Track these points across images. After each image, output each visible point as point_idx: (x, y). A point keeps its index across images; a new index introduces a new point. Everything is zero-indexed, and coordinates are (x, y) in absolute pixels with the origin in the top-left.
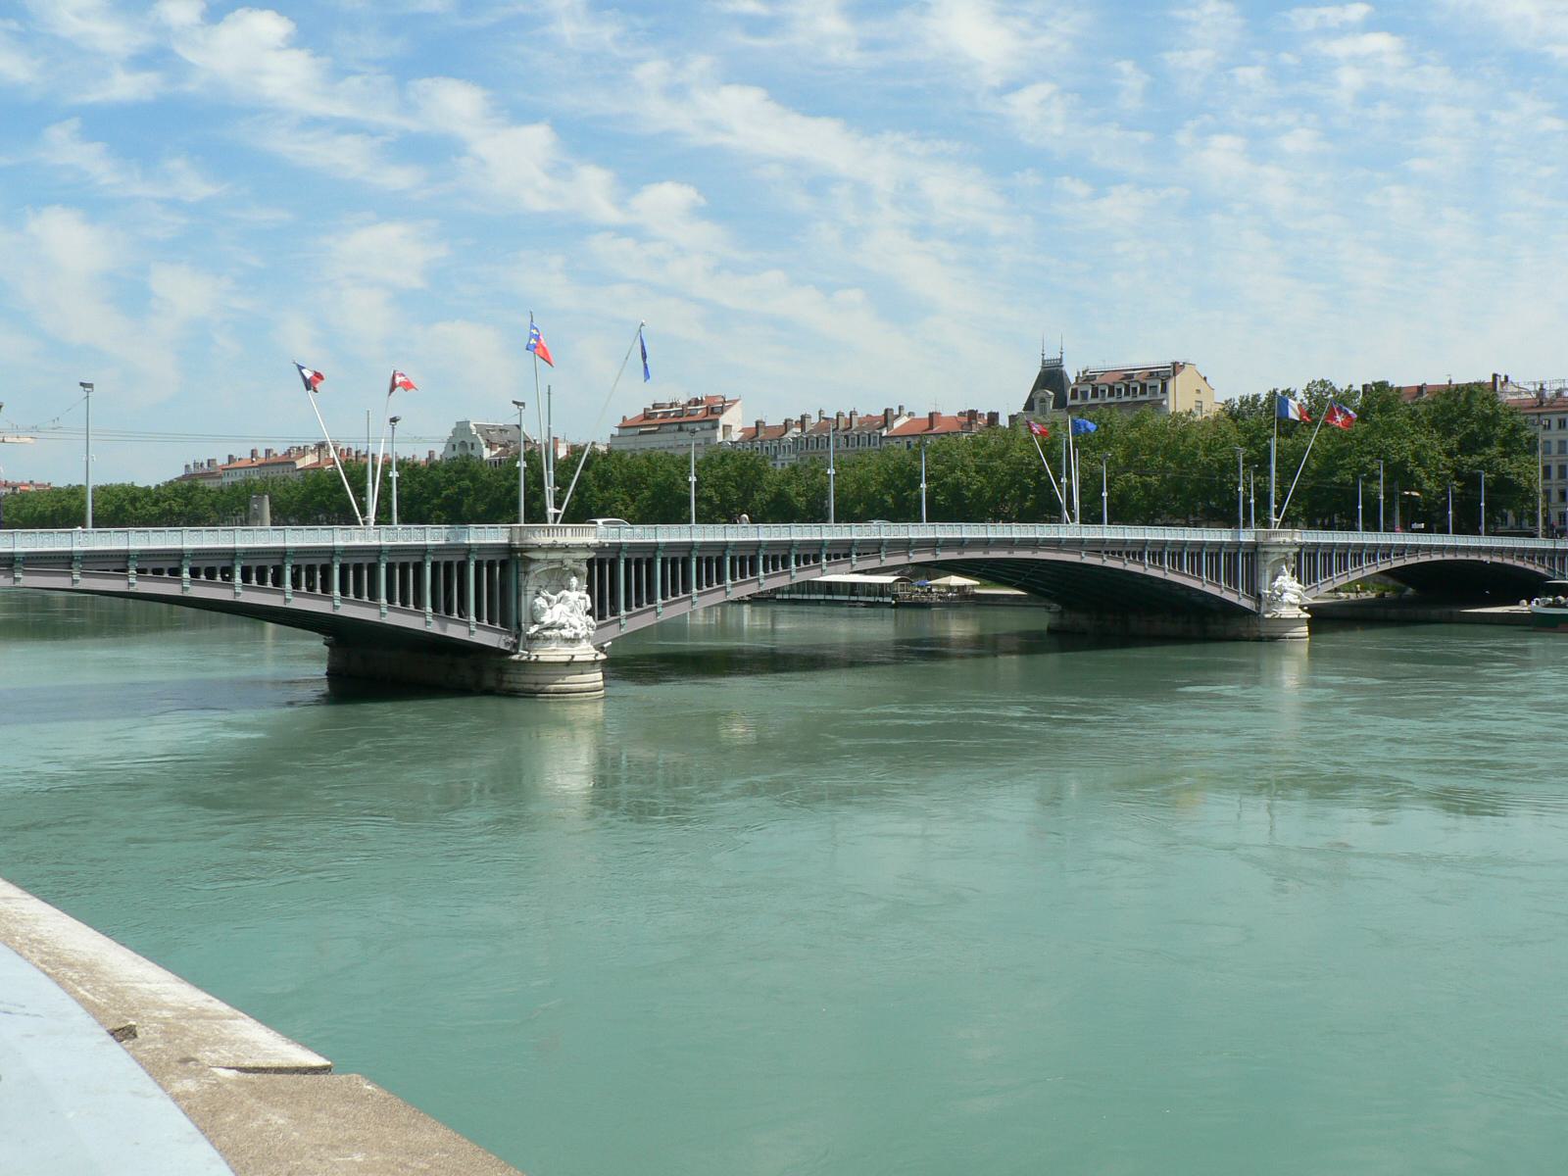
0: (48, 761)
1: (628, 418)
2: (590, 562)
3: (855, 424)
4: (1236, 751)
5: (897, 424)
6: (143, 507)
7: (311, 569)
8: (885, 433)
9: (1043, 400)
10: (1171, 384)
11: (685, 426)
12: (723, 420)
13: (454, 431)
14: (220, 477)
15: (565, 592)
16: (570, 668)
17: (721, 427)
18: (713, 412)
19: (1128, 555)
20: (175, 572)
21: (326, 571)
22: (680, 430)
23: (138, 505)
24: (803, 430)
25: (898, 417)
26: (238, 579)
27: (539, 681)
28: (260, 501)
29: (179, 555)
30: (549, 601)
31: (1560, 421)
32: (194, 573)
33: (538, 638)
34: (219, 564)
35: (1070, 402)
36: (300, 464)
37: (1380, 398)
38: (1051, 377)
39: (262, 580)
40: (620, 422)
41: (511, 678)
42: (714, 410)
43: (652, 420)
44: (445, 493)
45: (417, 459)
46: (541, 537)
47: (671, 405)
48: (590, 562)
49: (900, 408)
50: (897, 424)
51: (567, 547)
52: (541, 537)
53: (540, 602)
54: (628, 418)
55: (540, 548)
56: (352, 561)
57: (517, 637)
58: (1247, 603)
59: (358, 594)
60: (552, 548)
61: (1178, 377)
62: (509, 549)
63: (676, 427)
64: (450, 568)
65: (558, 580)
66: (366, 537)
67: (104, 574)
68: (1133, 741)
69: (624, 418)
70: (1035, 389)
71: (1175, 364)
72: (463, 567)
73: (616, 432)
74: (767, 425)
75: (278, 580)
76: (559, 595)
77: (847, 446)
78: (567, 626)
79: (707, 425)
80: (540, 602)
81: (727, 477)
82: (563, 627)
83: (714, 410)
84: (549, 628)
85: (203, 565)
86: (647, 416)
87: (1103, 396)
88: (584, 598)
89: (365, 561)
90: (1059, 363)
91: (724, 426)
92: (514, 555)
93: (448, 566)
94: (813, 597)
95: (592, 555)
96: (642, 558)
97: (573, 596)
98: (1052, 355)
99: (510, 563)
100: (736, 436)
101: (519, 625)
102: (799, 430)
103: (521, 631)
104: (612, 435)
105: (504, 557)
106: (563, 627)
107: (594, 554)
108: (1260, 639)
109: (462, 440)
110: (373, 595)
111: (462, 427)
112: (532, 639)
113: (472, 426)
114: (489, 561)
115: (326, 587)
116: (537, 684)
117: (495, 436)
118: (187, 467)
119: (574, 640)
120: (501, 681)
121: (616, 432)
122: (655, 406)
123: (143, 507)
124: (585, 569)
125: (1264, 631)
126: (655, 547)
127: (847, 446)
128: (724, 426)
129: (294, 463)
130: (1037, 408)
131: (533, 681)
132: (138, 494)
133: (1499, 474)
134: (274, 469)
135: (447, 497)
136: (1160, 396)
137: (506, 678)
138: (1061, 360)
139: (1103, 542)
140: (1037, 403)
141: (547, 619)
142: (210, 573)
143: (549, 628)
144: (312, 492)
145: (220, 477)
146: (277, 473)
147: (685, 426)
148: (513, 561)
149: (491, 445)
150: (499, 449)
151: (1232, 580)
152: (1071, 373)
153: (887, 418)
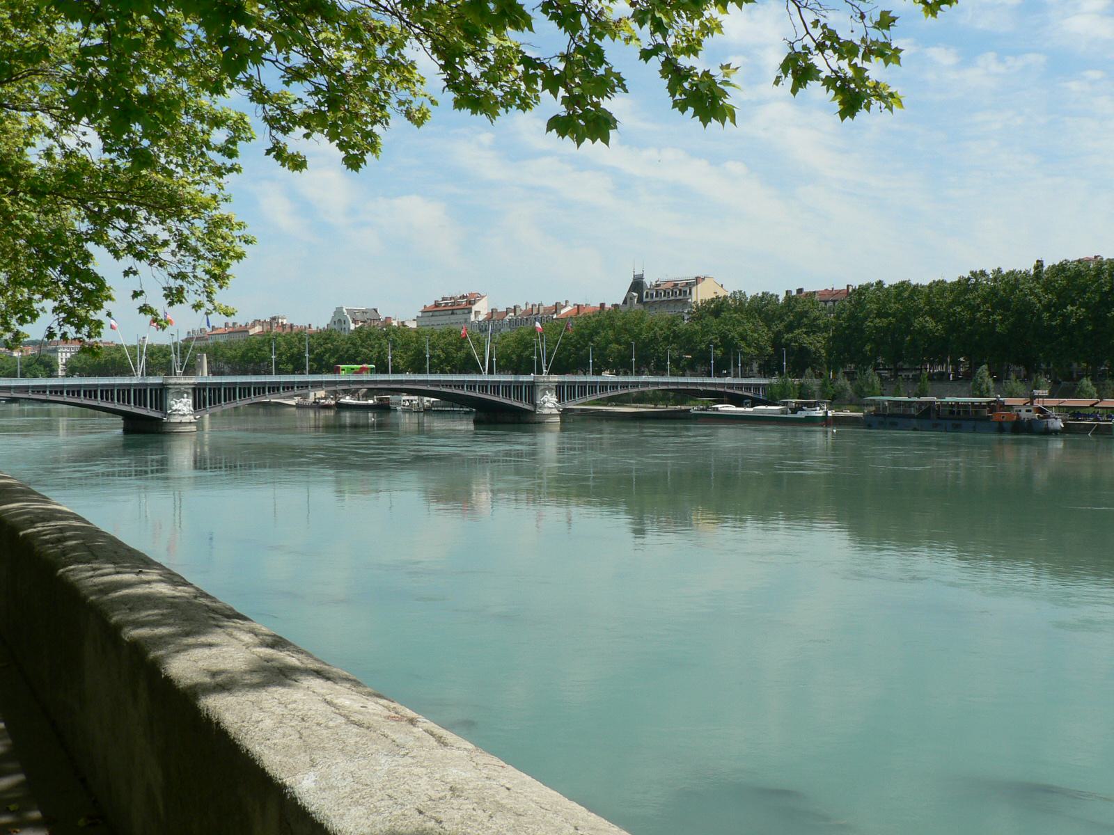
2: (556, 386)
3: (541, 311)
5: (563, 311)
6: (156, 359)
7: (483, 387)
8: (555, 316)
9: (631, 299)
10: (694, 289)
11: (455, 311)
12: (475, 308)
13: (335, 313)
14: (207, 340)
17: (473, 312)
18: (470, 304)
19: (455, 386)
20: (44, 392)
21: (96, 392)
22: (453, 314)
23: (155, 357)
24: (515, 314)
25: (565, 307)
26: (65, 394)
28: (201, 357)
29: (45, 387)
32: (51, 392)
34: (59, 390)
35: (645, 300)
36: (252, 332)
37: (904, 290)
38: (637, 285)
39: (73, 395)
42: (470, 301)
43: (436, 309)
44: (316, 352)
45: (321, 328)
46: (173, 380)
47: (451, 299)
48: (556, 386)
49: (567, 302)
50: (563, 311)
52: (173, 380)
53: (173, 402)
55: (170, 384)
56: (257, 386)
59: (107, 399)
60: (175, 384)
61: (699, 286)
62: (162, 384)
63: (450, 312)
64: (518, 386)
65: (180, 394)
66: (197, 379)
67: (21, 392)
68: (356, 448)
69: (425, 306)
71: (697, 278)
72: (145, 391)
73: (420, 314)
75: (79, 395)
79: (466, 311)
80: (173, 402)
81: (450, 344)
82: (179, 411)
83: (470, 301)
84: (175, 411)
85: (286, 386)
86: (437, 305)
89: (261, 386)
90: (641, 277)
91: (476, 312)
93: (140, 390)
94: (446, 409)
96: (572, 385)
97: (185, 400)
98: (638, 272)
99: (532, 387)
100: (481, 318)
102: (513, 314)
108: (535, 423)
109: (339, 319)
110: (112, 399)
111: (339, 311)
112: (170, 414)
113: (344, 310)
115: (96, 397)
117: (359, 316)
118: (189, 333)
119: (184, 415)
121: (420, 314)
122: (444, 299)
123: (156, 359)
124: (190, 391)
125: (537, 419)
126: (221, 384)
128: (476, 312)
129: (247, 331)
132: (156, 350)
133: (800, 344)
134: (237, 335)
135: (317, 354)
136: (688, 296)
139: (440, 381)
140: (628, 300)
141: (174, 408)
142: (288, 388)
143: (175, 411)
144: (247, 350)
145: (207, 340)
146: (236, 338)
147: (455, 311)
149: (355, 321)
150: (360, 324)
152: (649, 280)
153: (557, 307)
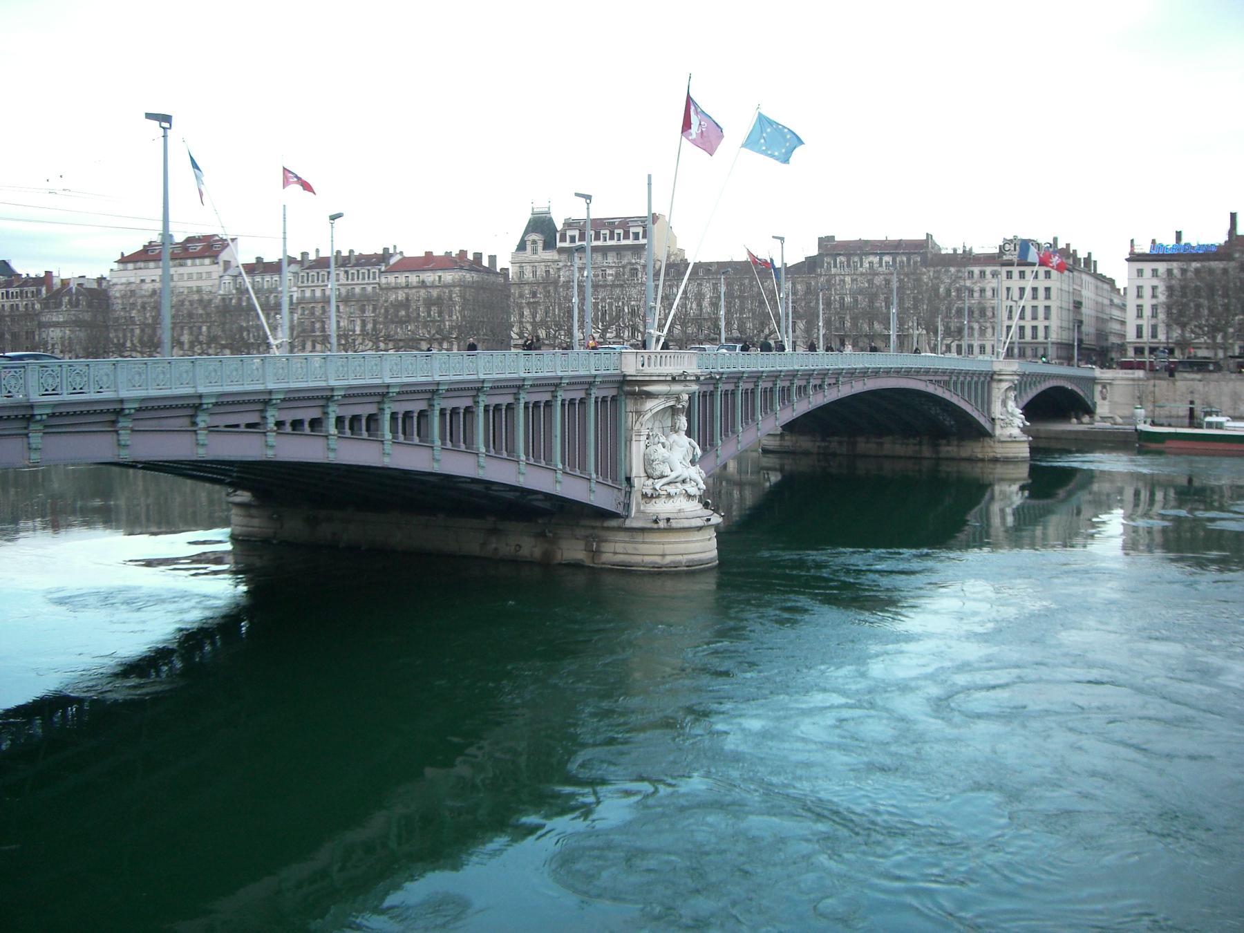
0: (1094, 674)
1: (126, 255)
4: (819, 815)
27: (667, 552)
31: (1008, 272)
35: (559, 245)
38: (541, 226)
40: (119, 257)
49: (395, 247)
54: (126, 255)
58: (602, 498)
69: (122, 254)
70: (526, 233)
74: (265, 261)
77: (347, 279)
87: (619, 240)
98: (541, 206)
101: (628, 479)
104: (112, 270)
116: (663, 555)
120: (596, 553)
127: (347, 279)
130: (529, 248)
138: (549, 208)
151: (575, 462)
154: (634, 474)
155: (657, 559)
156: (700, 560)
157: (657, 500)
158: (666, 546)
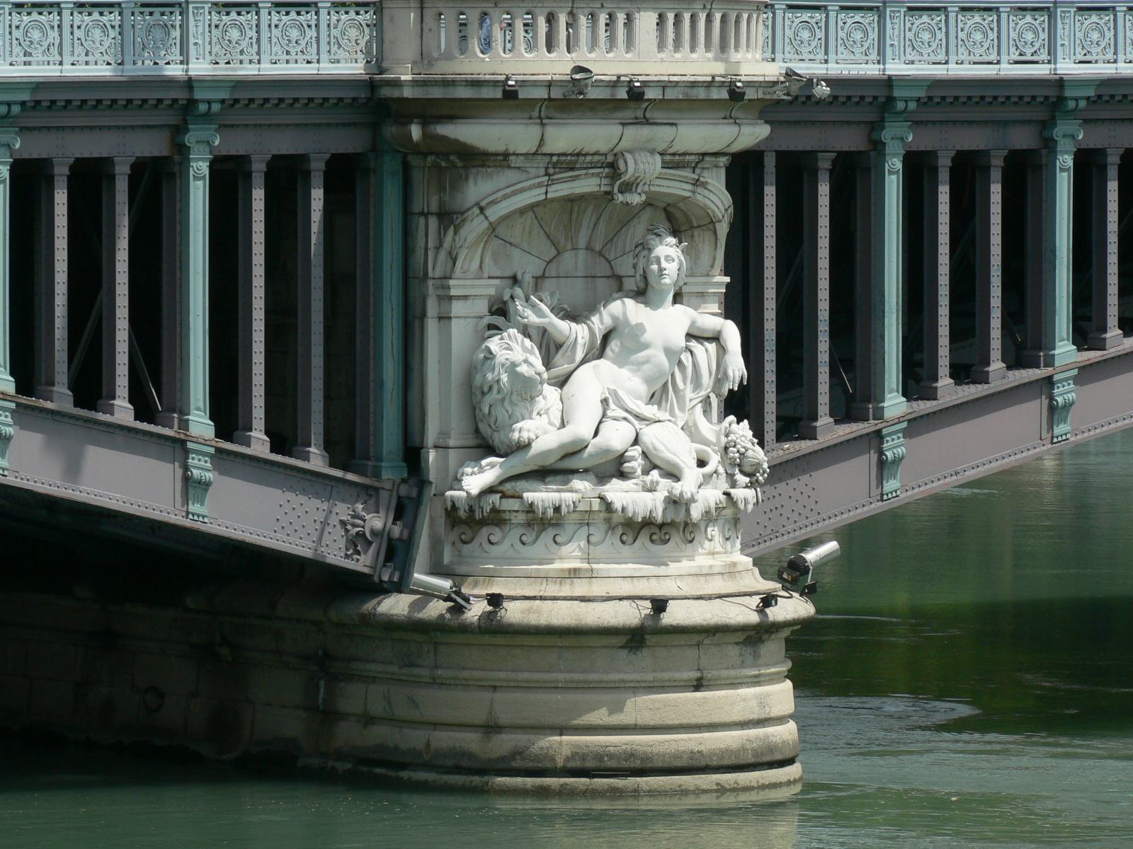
15: (627, 309)
16: (644, 656)
27: (504, 719)
30: (549, 347)
33: (497, 519)
41: (372, 698)
51: (636, 95)
57: (404, 510)
76: (600, 322)
78: (636, 464)
82: (615, 468)
88: (716, 338)
92: (390, 130)
95: (753, 134)
101: (413, 456)
103: (423, 483)
105: (349, 142)
106: (615, 468)
107: (763, 131)
114: (960, 153)
116: (491, 728)
131: (480, 717)
137: (353, 698)
148: (390, 165)
154: (431, 436)
155: (470, 741)
156: (631, 755)
157: (497, 534)
158: (498, 696)
